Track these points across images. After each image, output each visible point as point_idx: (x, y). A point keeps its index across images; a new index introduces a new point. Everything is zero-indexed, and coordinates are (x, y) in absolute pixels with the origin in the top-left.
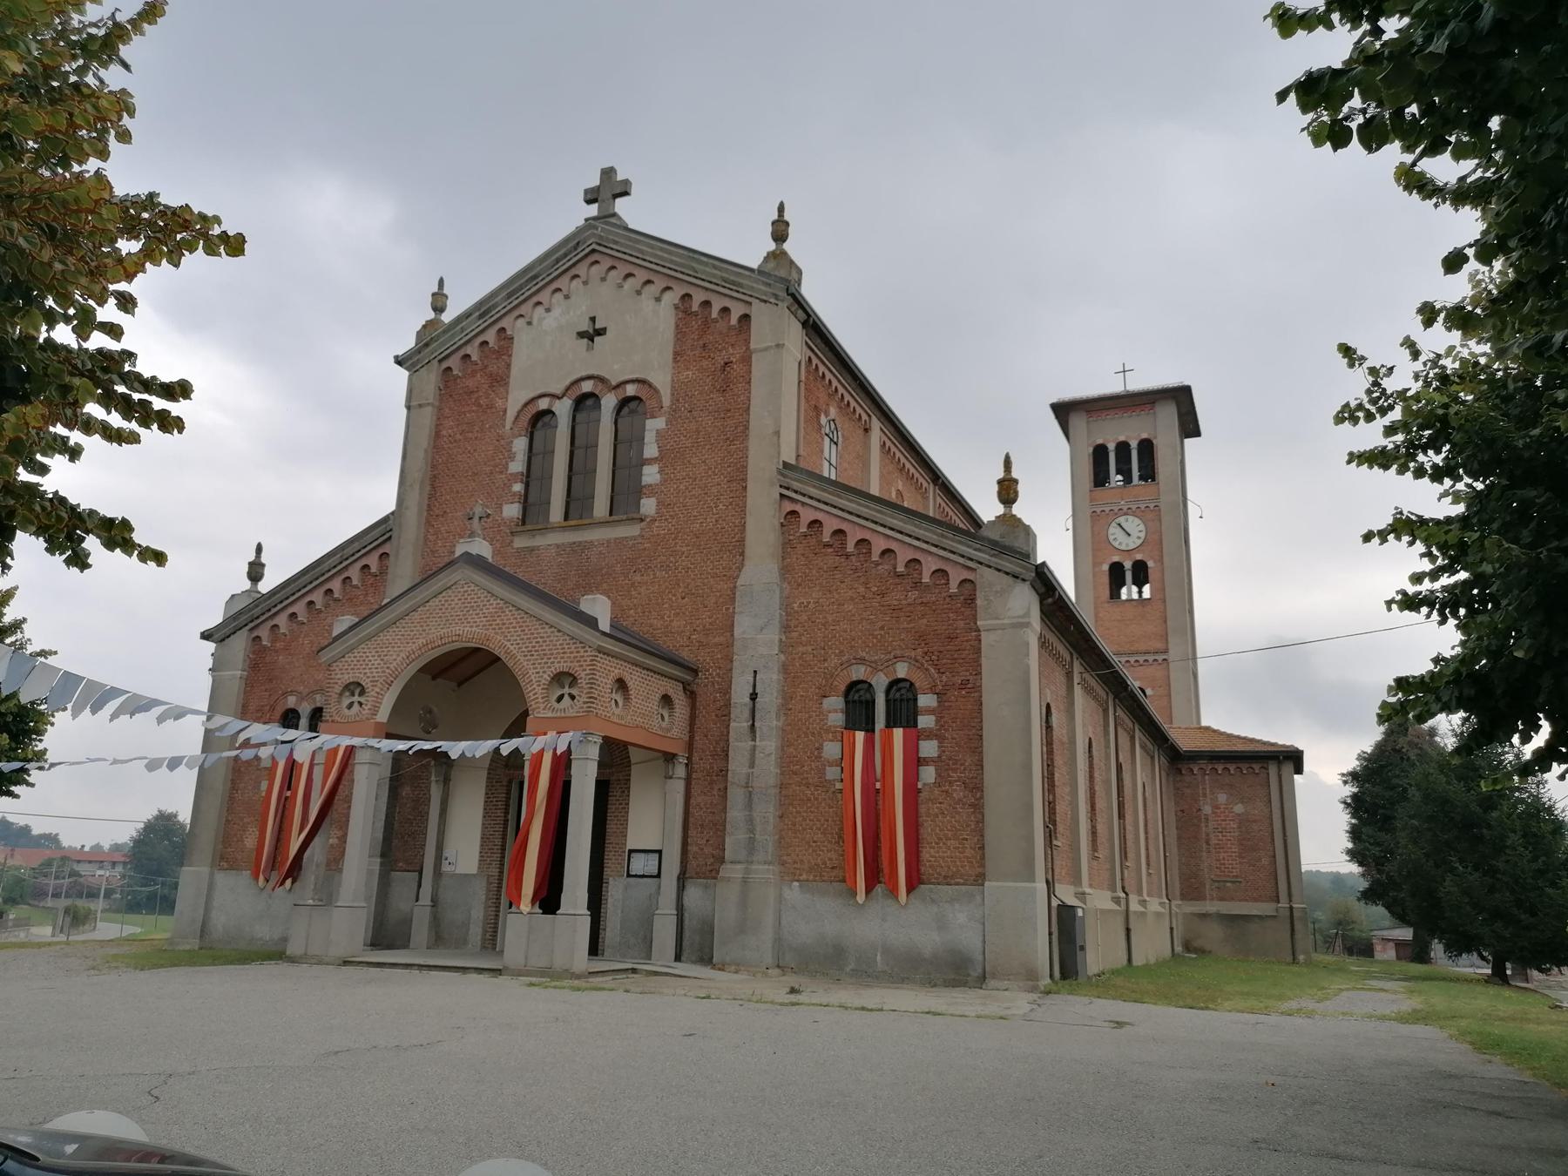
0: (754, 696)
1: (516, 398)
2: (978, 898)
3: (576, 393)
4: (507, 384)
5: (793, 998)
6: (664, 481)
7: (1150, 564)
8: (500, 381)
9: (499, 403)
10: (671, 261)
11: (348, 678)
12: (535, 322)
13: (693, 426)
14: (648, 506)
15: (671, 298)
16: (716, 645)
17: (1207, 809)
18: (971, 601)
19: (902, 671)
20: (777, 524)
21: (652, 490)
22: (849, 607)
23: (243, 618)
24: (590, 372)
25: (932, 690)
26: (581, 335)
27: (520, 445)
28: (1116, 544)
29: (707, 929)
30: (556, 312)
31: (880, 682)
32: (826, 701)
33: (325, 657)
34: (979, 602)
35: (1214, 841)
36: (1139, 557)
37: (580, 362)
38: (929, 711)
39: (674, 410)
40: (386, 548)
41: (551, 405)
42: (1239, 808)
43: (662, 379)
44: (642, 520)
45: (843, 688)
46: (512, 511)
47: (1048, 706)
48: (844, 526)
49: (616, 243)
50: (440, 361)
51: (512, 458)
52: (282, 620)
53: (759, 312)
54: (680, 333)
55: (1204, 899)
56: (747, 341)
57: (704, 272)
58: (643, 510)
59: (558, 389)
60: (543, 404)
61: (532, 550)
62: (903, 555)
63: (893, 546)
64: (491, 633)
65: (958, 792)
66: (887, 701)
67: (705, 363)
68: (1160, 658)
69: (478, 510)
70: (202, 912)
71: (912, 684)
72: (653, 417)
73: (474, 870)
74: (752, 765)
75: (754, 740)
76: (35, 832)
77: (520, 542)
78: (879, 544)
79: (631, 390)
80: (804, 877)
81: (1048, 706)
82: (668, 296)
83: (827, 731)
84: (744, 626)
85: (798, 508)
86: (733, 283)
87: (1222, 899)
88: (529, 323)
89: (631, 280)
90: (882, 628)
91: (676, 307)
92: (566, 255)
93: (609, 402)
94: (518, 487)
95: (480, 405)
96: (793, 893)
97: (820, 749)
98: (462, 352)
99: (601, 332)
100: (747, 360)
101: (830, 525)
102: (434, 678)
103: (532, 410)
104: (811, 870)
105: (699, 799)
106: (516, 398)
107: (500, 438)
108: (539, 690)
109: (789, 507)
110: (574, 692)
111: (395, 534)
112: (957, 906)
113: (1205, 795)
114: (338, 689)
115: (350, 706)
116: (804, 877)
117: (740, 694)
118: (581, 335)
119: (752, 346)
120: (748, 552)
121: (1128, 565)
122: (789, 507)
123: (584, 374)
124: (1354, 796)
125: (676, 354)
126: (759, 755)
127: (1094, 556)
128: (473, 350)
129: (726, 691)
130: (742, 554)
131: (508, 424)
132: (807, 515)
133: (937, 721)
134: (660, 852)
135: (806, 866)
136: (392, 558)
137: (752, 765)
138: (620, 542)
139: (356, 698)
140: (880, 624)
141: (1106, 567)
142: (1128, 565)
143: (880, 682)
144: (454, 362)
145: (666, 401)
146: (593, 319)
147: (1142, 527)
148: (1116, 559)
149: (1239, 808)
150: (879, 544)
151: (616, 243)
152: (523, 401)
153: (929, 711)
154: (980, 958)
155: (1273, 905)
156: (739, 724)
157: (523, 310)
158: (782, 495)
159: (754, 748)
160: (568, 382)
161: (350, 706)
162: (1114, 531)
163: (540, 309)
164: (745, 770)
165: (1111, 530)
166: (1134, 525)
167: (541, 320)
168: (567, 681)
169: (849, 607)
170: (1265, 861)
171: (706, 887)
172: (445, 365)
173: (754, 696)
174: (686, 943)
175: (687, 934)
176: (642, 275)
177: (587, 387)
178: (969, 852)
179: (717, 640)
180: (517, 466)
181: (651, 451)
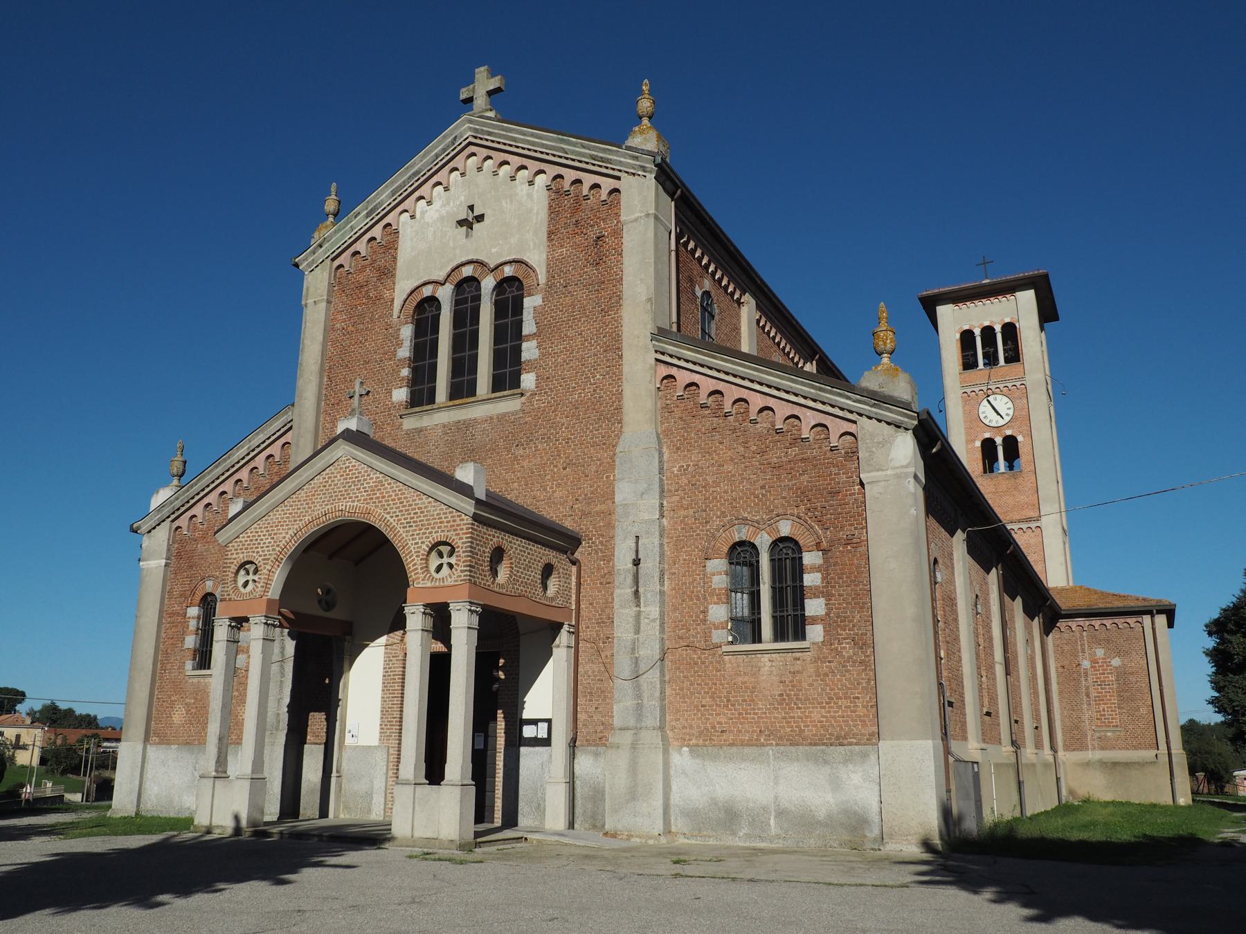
0: (637, 562)
1: (403, 286)
2: (873, 758)
3: (456, 278)
4: (393, 276)
5: (678, 869)
6: (543, 355)
7: (1020, 438)
8: (387, 273)
9: (387, 294)
10: (543, 146)
11: (242, 557)
12: (418, 215)
13: (568, 300)
14: (528, 380)
15: (541, 180)
16: (598, 514)
17: (1086, 664)
18: (853, 454)
19: (785, 529)
20: (652, 388)
21: (533, 366)
22: (729, 467)
23: (166, 511)
24: (470, 258)
25: (818, 546)
26: (461, 223)
27: (407, 332)
28: (987, 422)
29: (598, 795)
30: (437, 204)
31: (763, 541)
32: (709, 564)
33: (222, 537)
34: (861, 455)
35: (1093, 694)
36: (1009, 432)
37: (462, 248)
38: (815, 569)
39: (550, 286)
40: (288, 437)
41: (434, 291)
42: (1116, 662)
43: (537, 258)
44: (522, 395)
45: (725, 549)
46: (401, 395)
47: (936, 561)
48: (721, 386)
49: (490, 134)
50: (333, 260)
51: (400, 345)
52: (198, 510)
53: (626, 183)
54: (554, 211)
55: (1087, 749)
56: (618, 215)
57: (573, 152)
58: (523, 385)
59: (440, 275)
60: (427, 291)
61: (419, 431)
62: (783, 410)
63: (771, 402)
64: (371, 507)
65: (848, 650)
66: (772, 560)
67: (578, 239)
68: (1033, 525)
69: (358, 389)
70: (137, 783)
71: (796, 543)
72: (530, 295)
73: (375, 742)
74: (637, 631)
75: (638, 606)
76: (77, 713)
77: (409, 423)
78: (757, 401)
79: (508, 271)
80: (694, 741)
81: (936, 561)
82: (541, 180)
83: (712, 594)
84: (624, 492)
85: (674, 371)
86: (602, 160)
87: (1103, 749)
88: (413, 217)
89: (506, 167)
90: (763, 487)
91: (549, 188)
92: (444, 150)
93: (488, 283)
94: (405, 372)
95: (369, 298)
96: (681, 759)
97: (705, 612)
98: (352, 250)
99: (480, 218)
100: (617, 233)
101: (707, 385)
102: (330, 557)
103: (417, 298)
104: (701, 733)
105: (587, 668)
106: (403, 286)
107: (388, 326)
108: (418, 561)
109: (664, 371)
110: (453, 560)
111: (294, 424)
112: (851, 767)
113: (1083, 651)
114: (234, 568)
115: (246, 584)
116: (694, 741)
117: (623, 560)
118: (461, 223)
119: (623, 218)
120: (626, 419)
121: (999, 440)
122: (664, 371)
123: (464, 259)
124: (1215, 649)
125: (550, 233)
126: (644, 621)
127: (968, 434)
128: (361, 246)
129: (609, 558)
130: (620, 422)
131: (395, 316)
132: (683, 377)
133: (823, 579)
134: (549, 721)
135: (695, 731)
136: (293, 447)
137: (637, 631)
138: (502, 417)
139: (251, 577)
140: (761, 483)
141: (978, 444)
142: (999, 440)
143: (763, 541)
144: (344, 259)
145: (542, 279)
146: (471, 208)
147: (1010, 405)
148: (987, 435)
149: (1116, 662)
150: (757, 401)
151: (490, 134)
152: (408, 291)
153: (815, 569)
154: (877, 819)
155: (1153, 753)
156: (623, 591)
157: (407, 204)
158: (657, 360)
159: (638, 614)
160: (449, 269)
161: (246, 584)
162: (985, 409)
163: (422, 203)
164: (631, 636)
165: (981, 409)
166: (1002, 403)
167: (423, 213)
168: (445, 549)
169: (729, 467)
170: (1144, 711)
171: (597, 755)
172: (336, 263)
173: (637, 562)
174: (578, 811)
175: (579, 802)
176: (516, 161)
177: (467, 271)
178: (861, 711)
179: (598, 508)
180: (405, 352)
181: (528, 327)
